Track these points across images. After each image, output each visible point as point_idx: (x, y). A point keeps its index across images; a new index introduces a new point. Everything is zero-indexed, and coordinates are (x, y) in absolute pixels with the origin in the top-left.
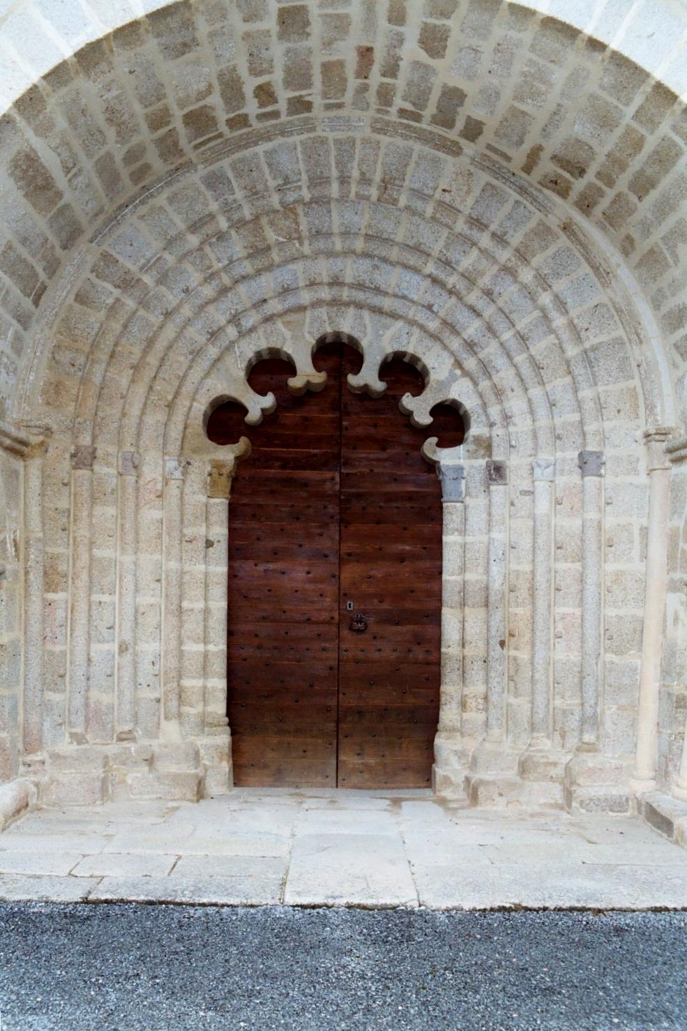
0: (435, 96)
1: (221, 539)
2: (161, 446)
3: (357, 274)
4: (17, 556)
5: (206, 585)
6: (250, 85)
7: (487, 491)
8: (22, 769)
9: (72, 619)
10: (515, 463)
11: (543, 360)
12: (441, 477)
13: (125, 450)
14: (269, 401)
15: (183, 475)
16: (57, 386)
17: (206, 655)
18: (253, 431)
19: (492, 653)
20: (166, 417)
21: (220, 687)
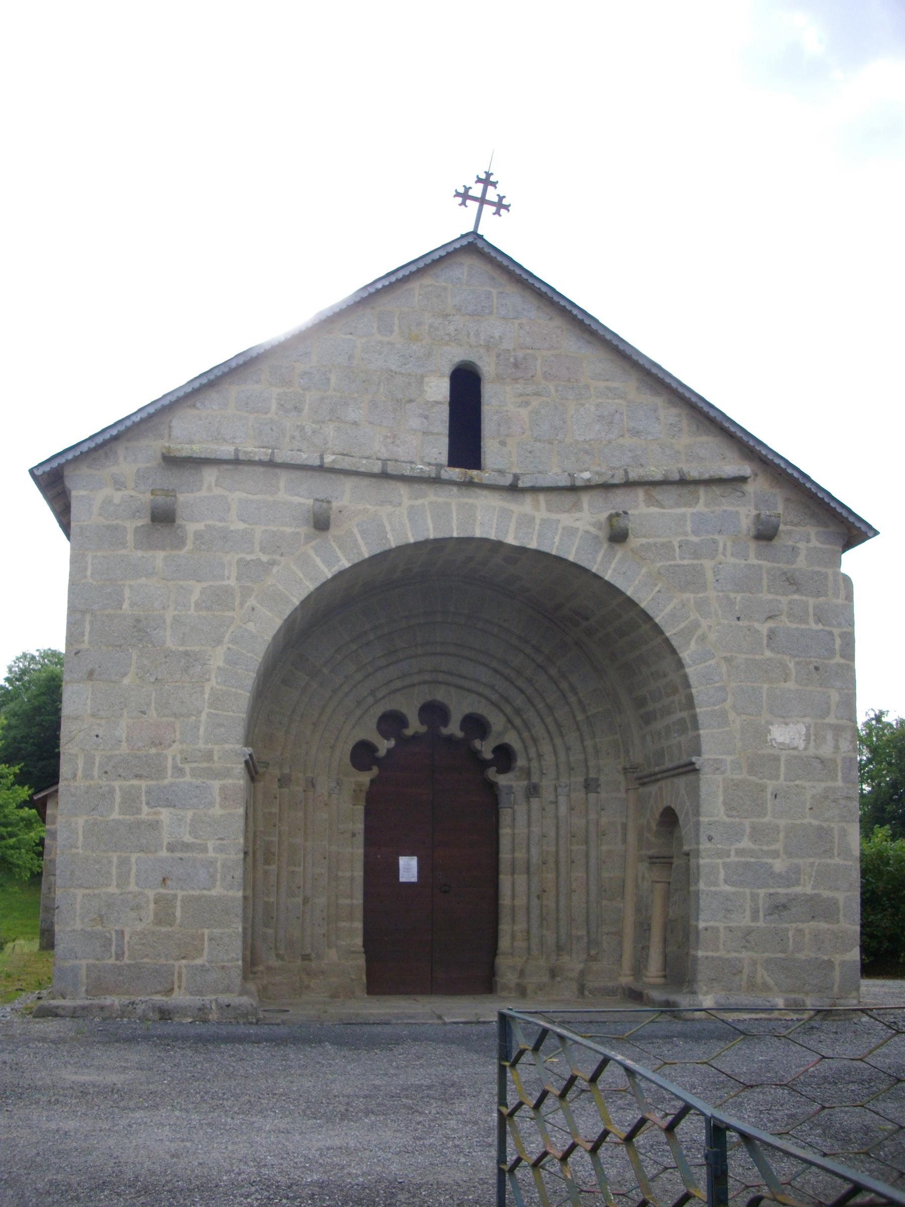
10: (546, 784)
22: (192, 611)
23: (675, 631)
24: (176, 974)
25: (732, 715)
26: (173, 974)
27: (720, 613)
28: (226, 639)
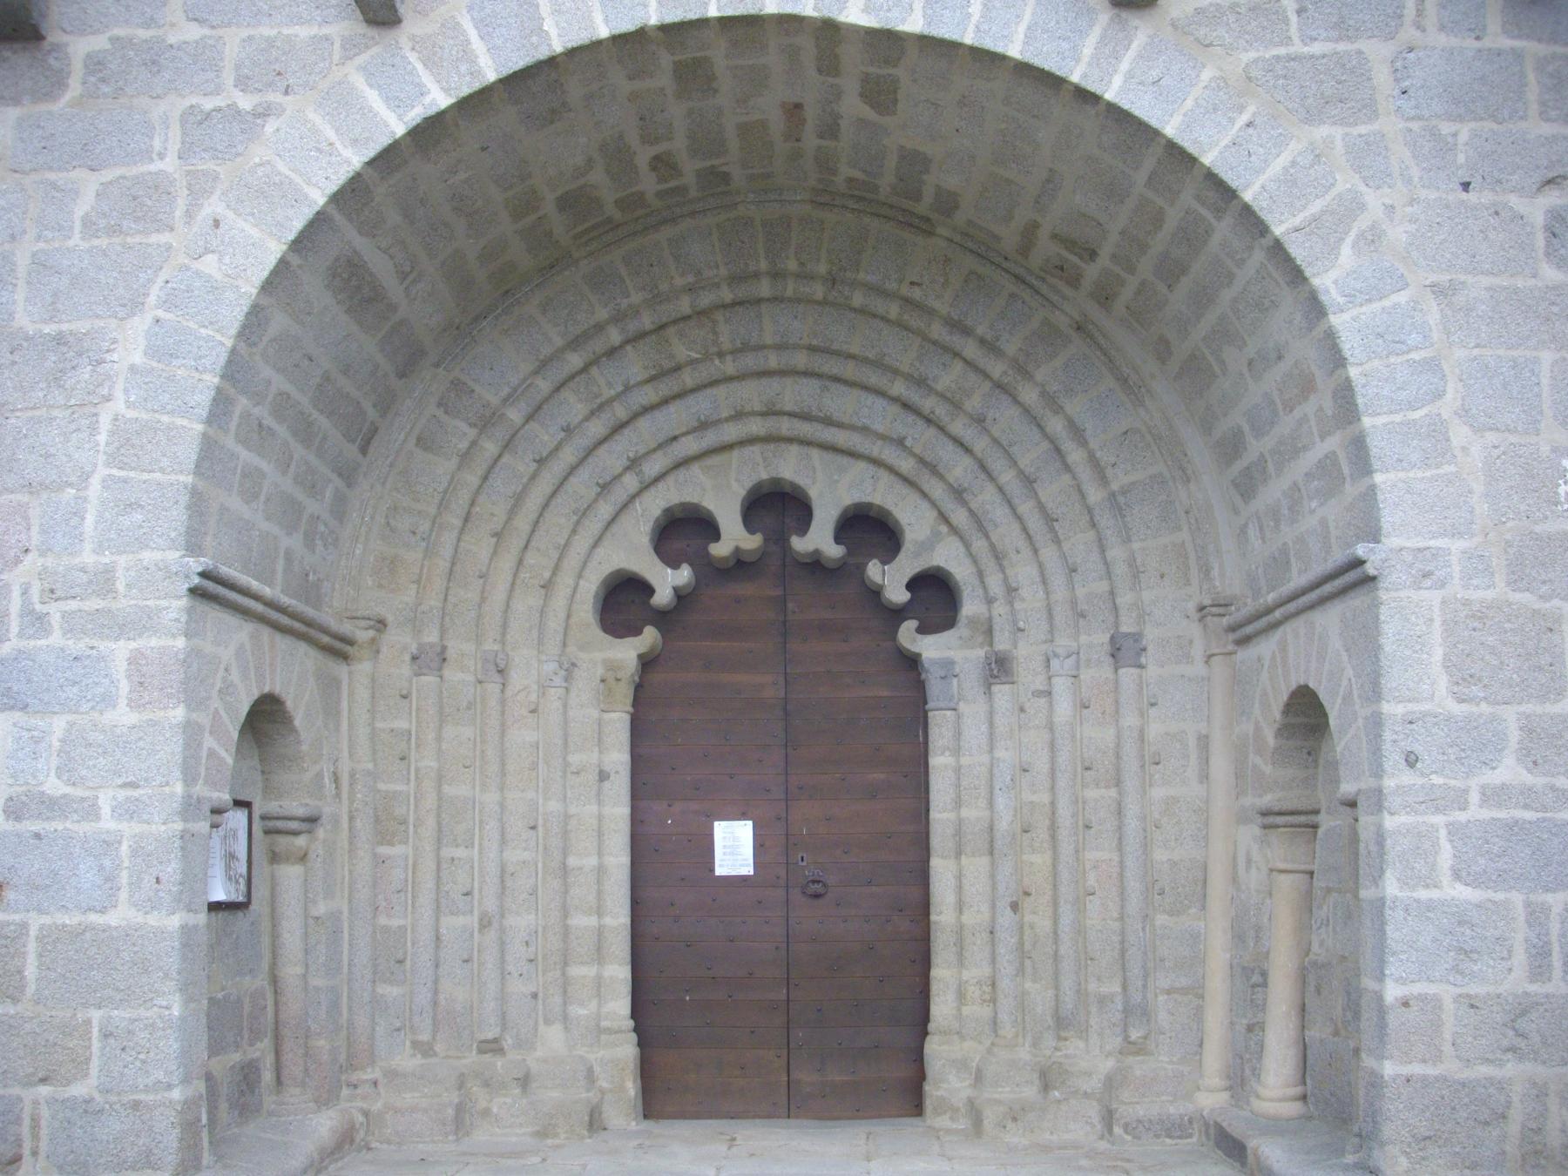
0: (891, 162)
4: (338, 795)
5: (600, 834)
6: (644, 156)
7: (988, 691)
8: (345, 1092)
10: (1027, 654)
12: (923, 676)
14: (684, 575)
17: (600, 931)
18: (662, 619)
19: (1000, 920)
21: (622, 976)
22: (76, 240)
23: (1297, 221)
24: (27, 1122)
25: (1460, 434)
26: (18, 1121)
27: (1415, 172)
28: (152, 299)
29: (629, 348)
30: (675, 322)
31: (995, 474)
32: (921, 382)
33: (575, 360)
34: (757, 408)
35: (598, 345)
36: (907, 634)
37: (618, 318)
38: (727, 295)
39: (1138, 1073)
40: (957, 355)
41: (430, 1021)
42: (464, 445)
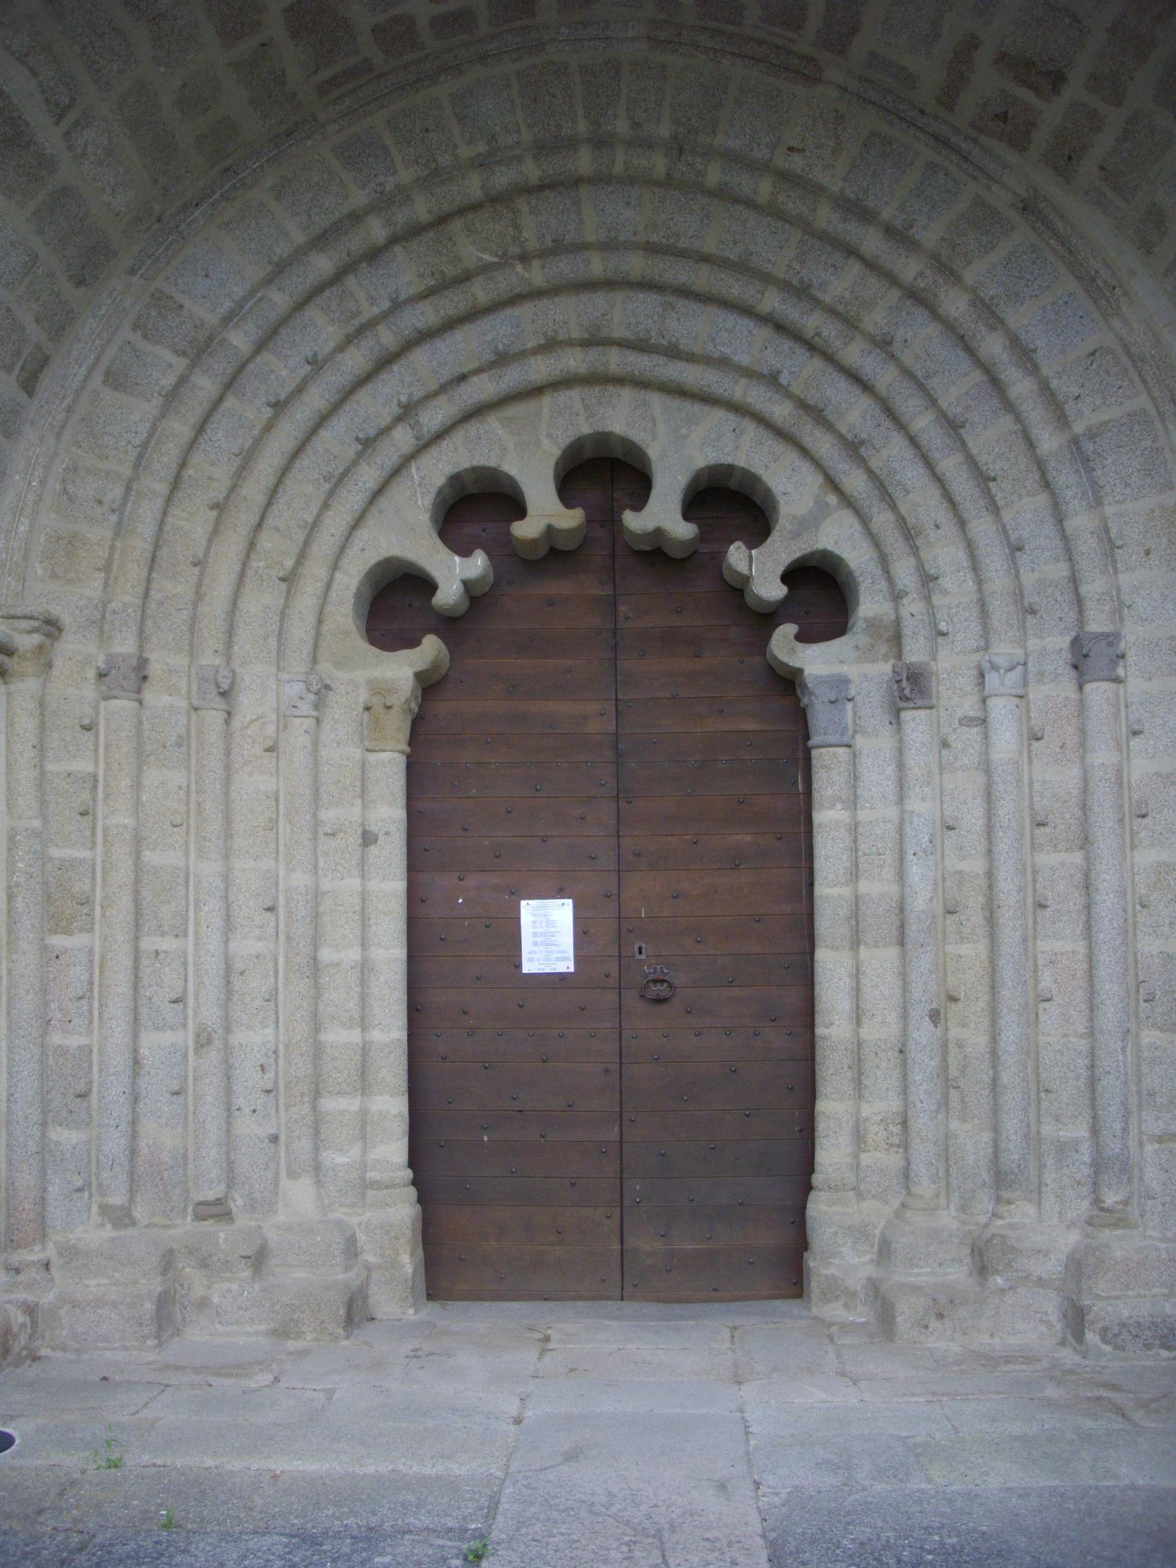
1: (393, 829)
2: (274, 654)
3: (632, 320)
9: (101, 985)
10: (950, 667)
11: (994, 462)
12: (805, 701)
13: (204, 662)
14: (477, 564)
15: (316, 707)
16: (70, 542)
17: (365, 1050)
18: (449, 625)
20: (282, 601)
21: (394, 1111)
29: (397, 249)
30: (461, 212)
31: (905, 419)
32: (802, 292)
33: (323, 264)
34: (575, 334)
35: (354, 243)
36: (784, 643)
37: (382, 204)
38: (531, 171)
39: (1119, 1254)
40: (852, 252)
41: (123, 1178)
42: (169, 381)
